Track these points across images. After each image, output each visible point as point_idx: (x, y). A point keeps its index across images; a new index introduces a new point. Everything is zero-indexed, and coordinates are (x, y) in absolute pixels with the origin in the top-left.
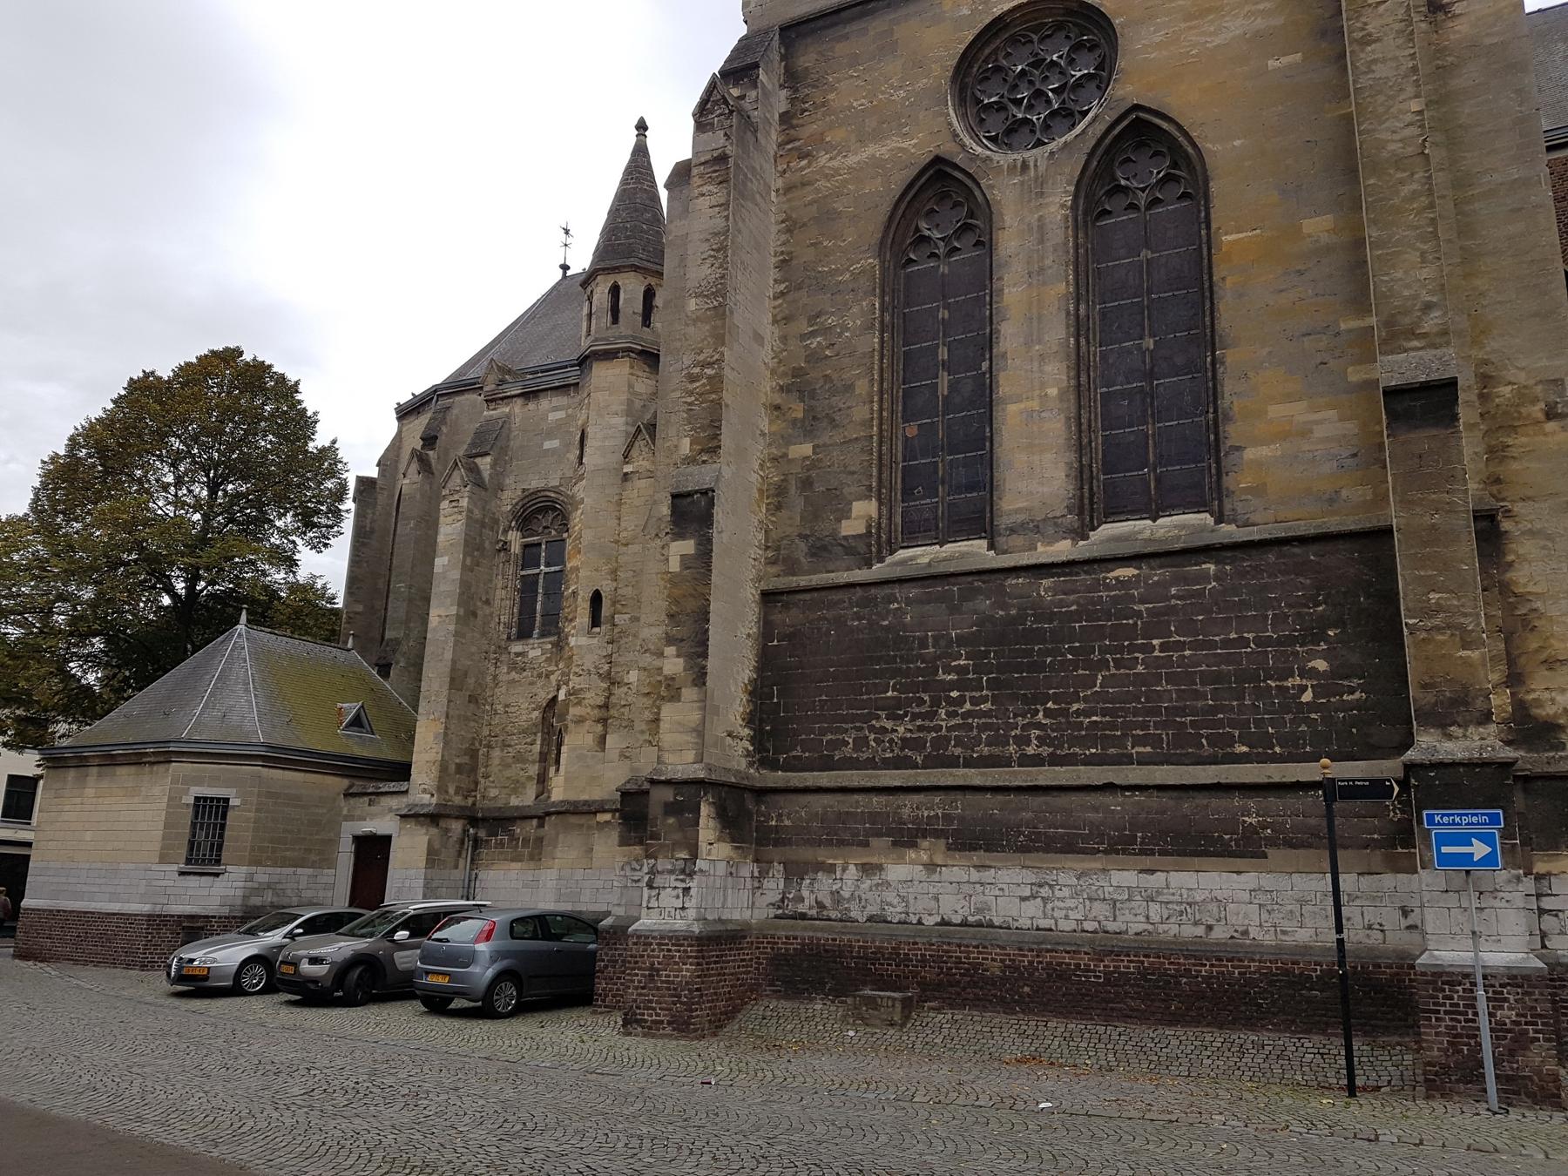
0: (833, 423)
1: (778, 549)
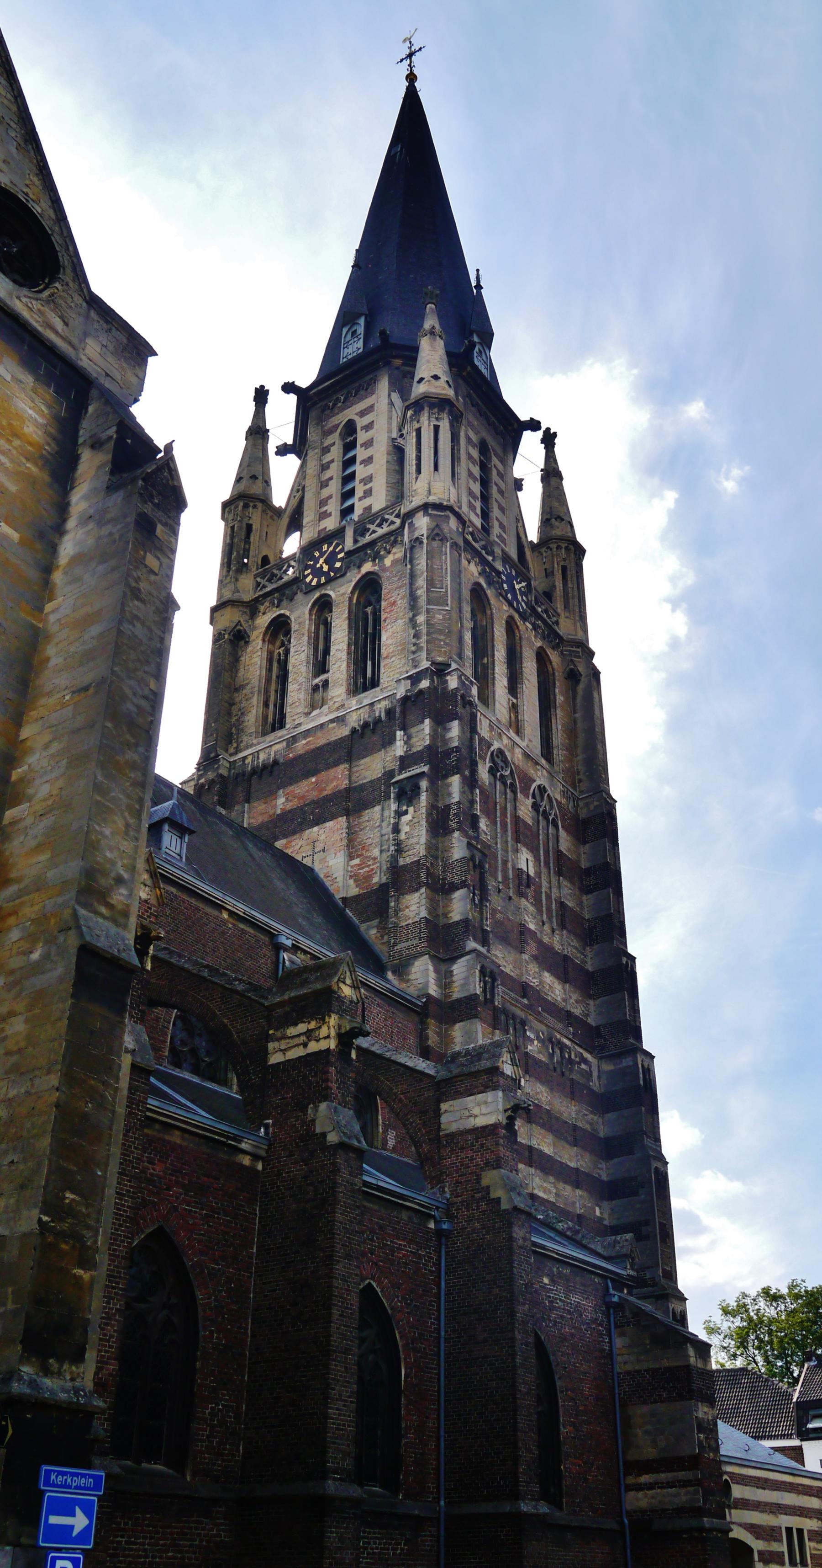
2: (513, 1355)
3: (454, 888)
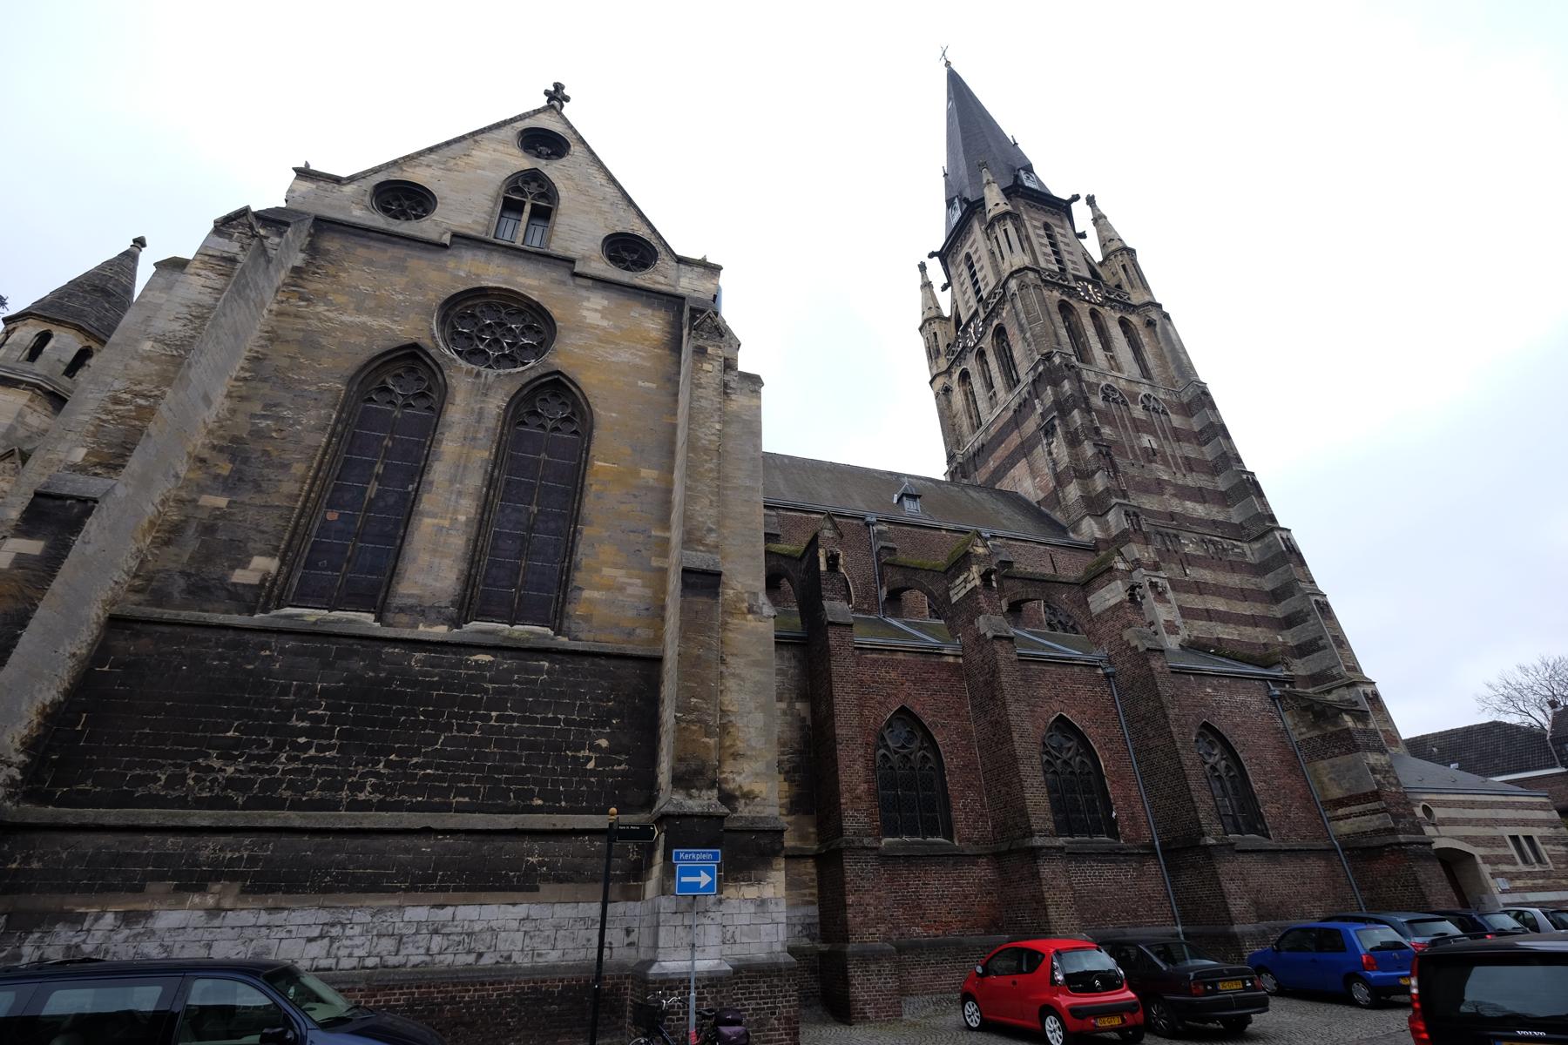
0: (258, 488)
1: (150, 580)
2: (1174, 742)
3: (1094, 473)
